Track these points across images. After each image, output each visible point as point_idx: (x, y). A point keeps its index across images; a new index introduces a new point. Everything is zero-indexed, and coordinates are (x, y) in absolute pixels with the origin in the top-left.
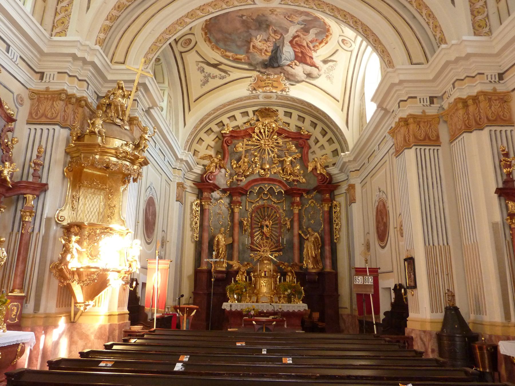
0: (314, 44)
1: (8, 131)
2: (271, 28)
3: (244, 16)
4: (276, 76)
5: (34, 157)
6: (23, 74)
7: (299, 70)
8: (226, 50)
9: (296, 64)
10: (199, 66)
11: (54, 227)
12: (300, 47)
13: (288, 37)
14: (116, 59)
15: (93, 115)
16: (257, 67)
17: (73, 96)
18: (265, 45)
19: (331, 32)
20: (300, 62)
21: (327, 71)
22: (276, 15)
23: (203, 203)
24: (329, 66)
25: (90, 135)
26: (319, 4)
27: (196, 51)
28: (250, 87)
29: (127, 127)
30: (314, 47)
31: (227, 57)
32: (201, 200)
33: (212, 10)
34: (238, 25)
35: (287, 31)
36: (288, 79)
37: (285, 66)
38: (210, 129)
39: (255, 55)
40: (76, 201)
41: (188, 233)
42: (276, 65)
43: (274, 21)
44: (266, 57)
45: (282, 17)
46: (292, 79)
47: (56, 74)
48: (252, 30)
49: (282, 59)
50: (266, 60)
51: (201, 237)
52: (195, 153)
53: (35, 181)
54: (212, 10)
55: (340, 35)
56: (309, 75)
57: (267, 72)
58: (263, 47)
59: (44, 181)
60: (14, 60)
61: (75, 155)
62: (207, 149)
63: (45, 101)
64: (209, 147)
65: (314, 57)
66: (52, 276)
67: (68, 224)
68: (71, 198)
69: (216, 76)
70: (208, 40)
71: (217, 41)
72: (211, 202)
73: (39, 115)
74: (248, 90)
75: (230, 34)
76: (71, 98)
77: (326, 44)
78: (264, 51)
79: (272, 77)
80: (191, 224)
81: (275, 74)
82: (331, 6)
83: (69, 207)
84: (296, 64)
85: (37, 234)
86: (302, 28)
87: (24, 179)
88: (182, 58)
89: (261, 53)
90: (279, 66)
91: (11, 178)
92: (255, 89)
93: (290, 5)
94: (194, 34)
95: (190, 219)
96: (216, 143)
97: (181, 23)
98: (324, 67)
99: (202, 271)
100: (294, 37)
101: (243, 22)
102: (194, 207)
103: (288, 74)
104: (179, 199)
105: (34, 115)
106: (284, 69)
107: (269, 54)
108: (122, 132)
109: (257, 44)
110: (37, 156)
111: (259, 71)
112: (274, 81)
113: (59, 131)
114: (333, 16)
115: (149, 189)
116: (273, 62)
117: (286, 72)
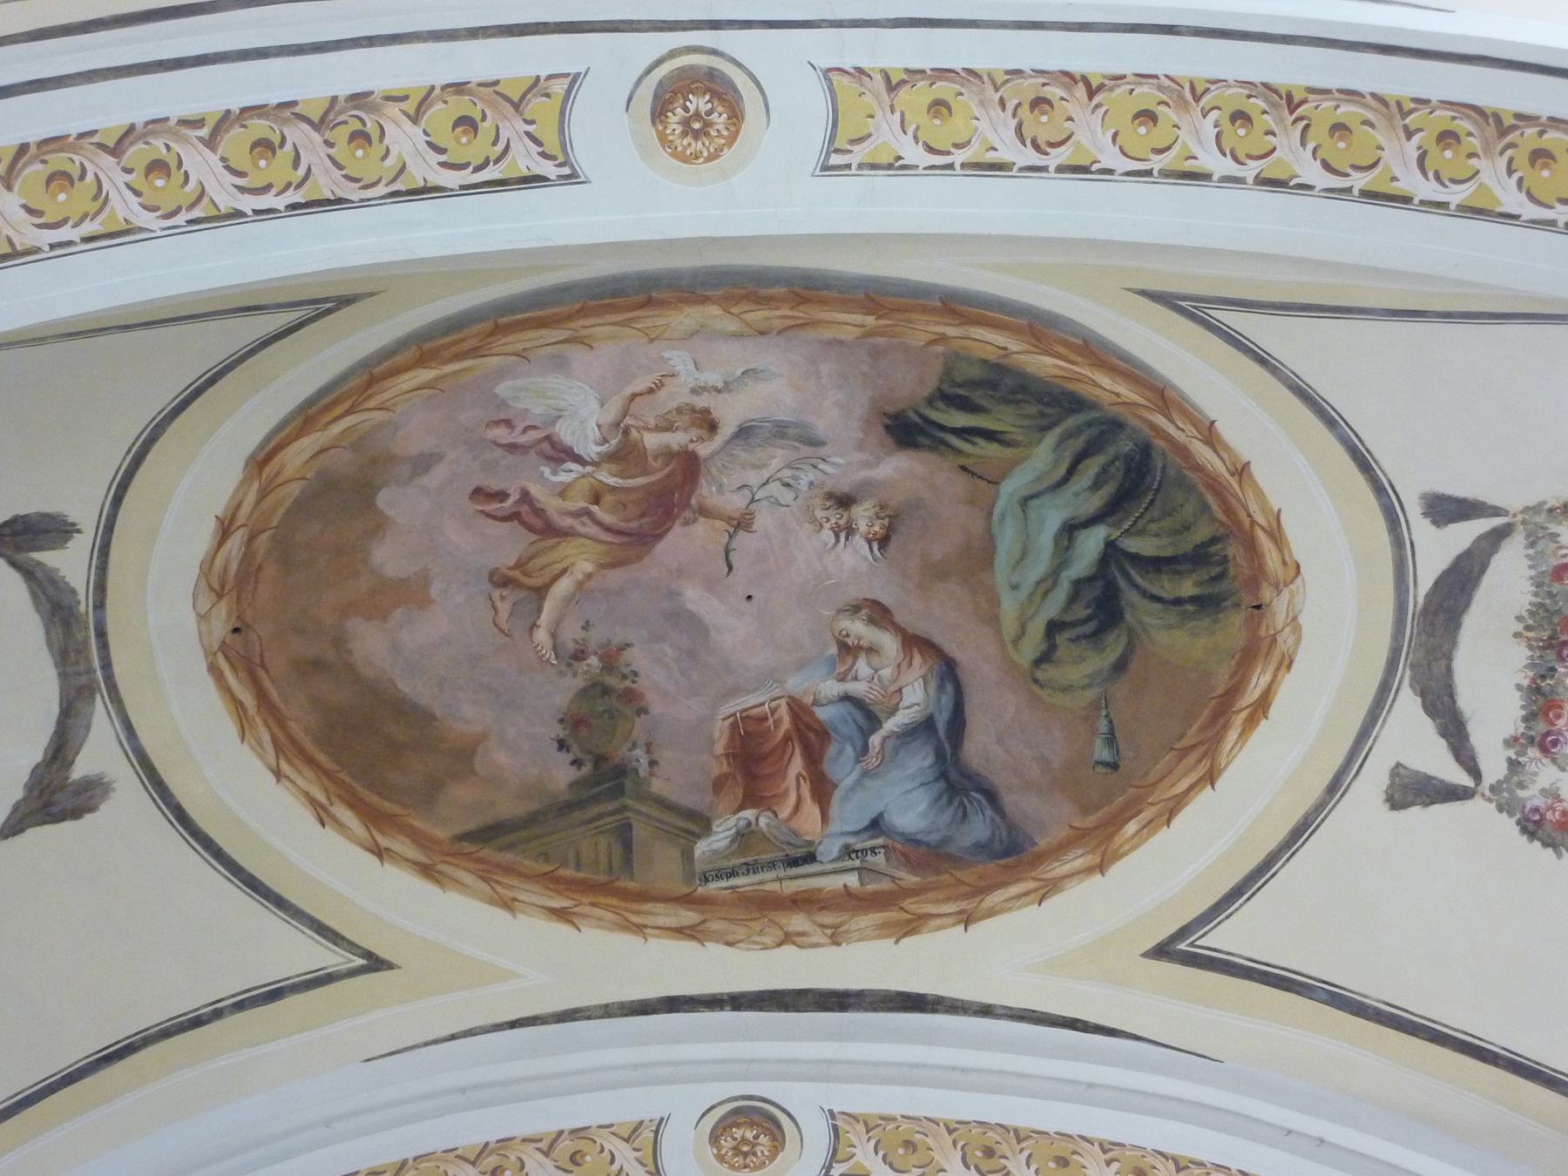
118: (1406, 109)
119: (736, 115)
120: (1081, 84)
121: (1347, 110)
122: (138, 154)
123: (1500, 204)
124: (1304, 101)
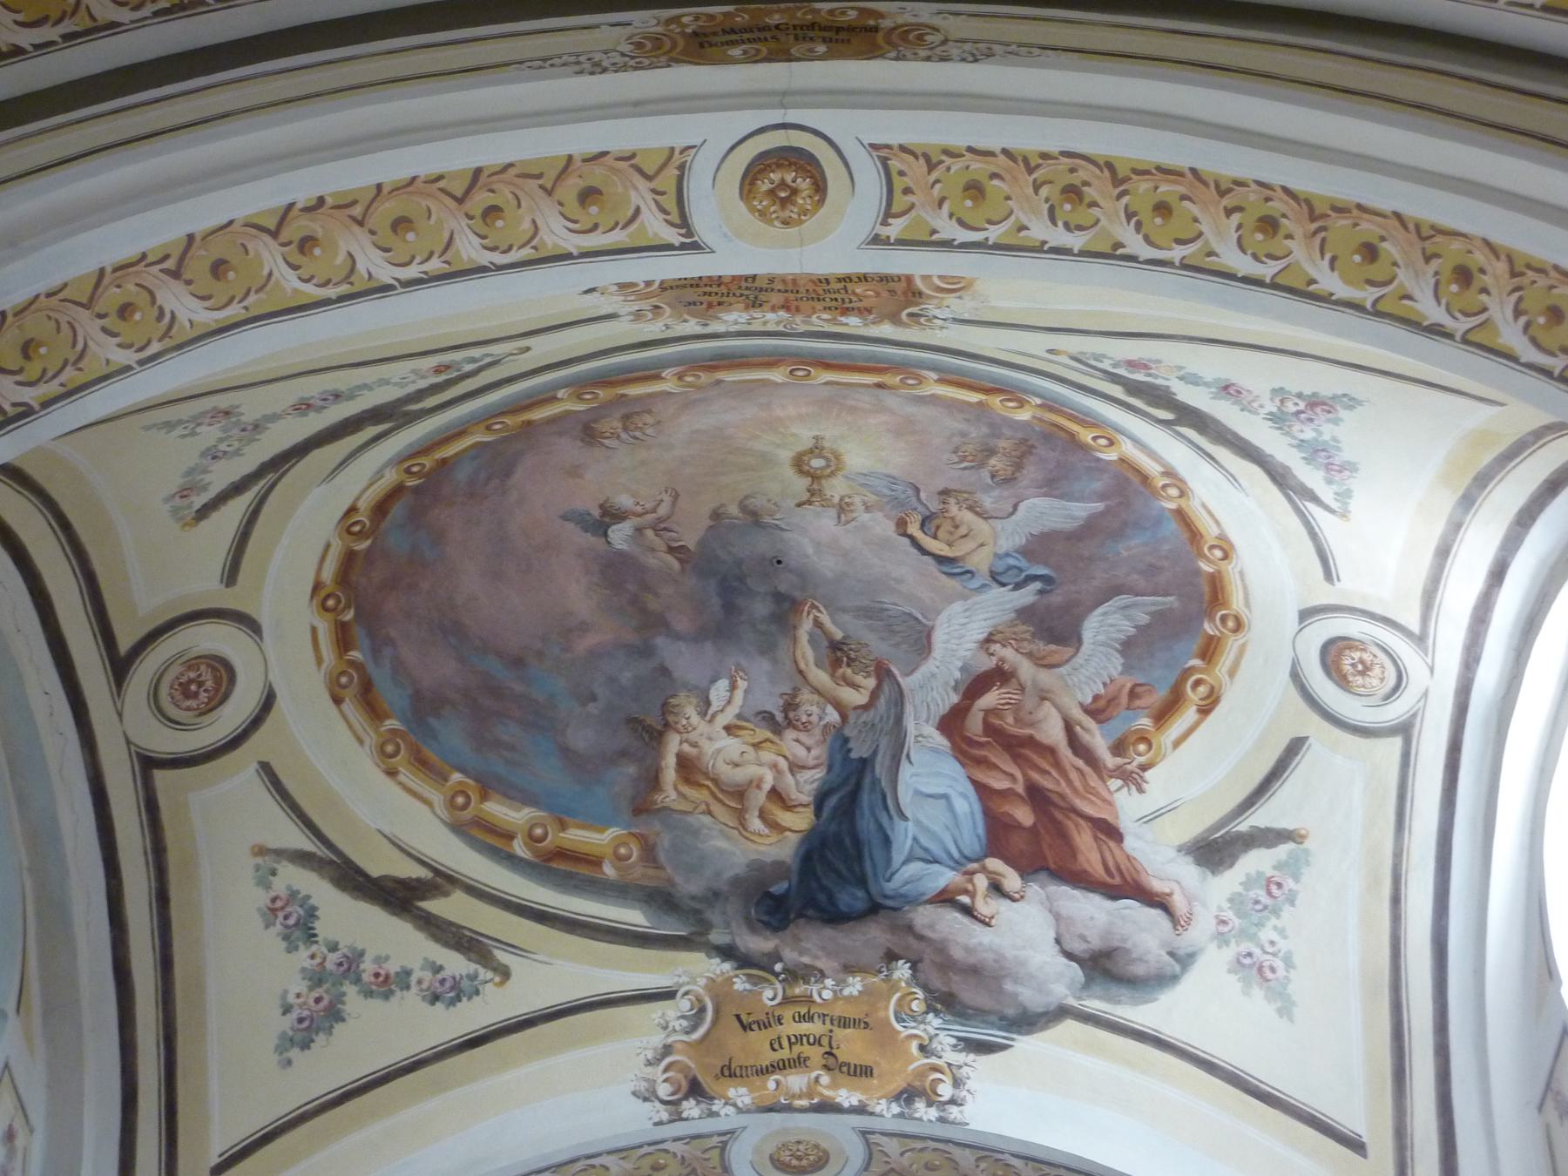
0: (1120, 724)
2: (806, 626)
3: (619, 516)
4: (855, 985)
7: (1026, 929)
8: (487, 786)
9: (997, 888)
10: (279, 886)
12: (1017, 758)
13: (930, 687)
16: (713, 916)
18: (767, 756)
19: (1237, 603)
20: (1030, 867)
21: (1236, 922)
22: (843, 508)
24: (1248, 884)
26: (1163, 209)
27: (266, 769)
28: (657, 1073)
30: (1119, 748)
31: (490, 839)
33: (374, 265)
34: (578, 595)
35: (921, 643)
36: (945, 1002)
37: (915, 901)
39: (696, 833)
42: (850, 898)
43: (827, 565)
44: (775, 843)
45: (884, 526)
46: (988, 1010)
48: (678, 637)
49: (898, 856)
50: (779, 868)
54: (374, 265)
55: (1306, 615)
56: (1103, 966)
57: (790, 955)
58: (751, 771)
65: (1126, 823)
70: (358, 691)
71: (425, 707)
74: (648, 1096)
75: (518, 663)
77: (1205, 711)
78: (759, 798)
79: (824, 992)
81: (849, 969)
82: (1253, 196)
84: (997, 888)
86: (1025, 614)
88: (151, 806)
89: (740, 815)
90: (874, 909)
92: (695, 1089)
93: (947, 245)
94: (250, 624)
97: (125, 311)
98: (1213, 896)
100: (977, 685)
101: (616, 573)
103: (947, 965)
106: (910, 928)
107: (800, 821)
109: (709, 748)
111: (727, 952)
112: (844, 1023)
114: (1274, 286)
116: (832, 879)
117: (929, 955)
118: (1033, 164)
119: (820, 187)
120: (922, 161)
121: (978, 167)
122: (573, 185)
123: (1426, 318)
124: (1038, 166)
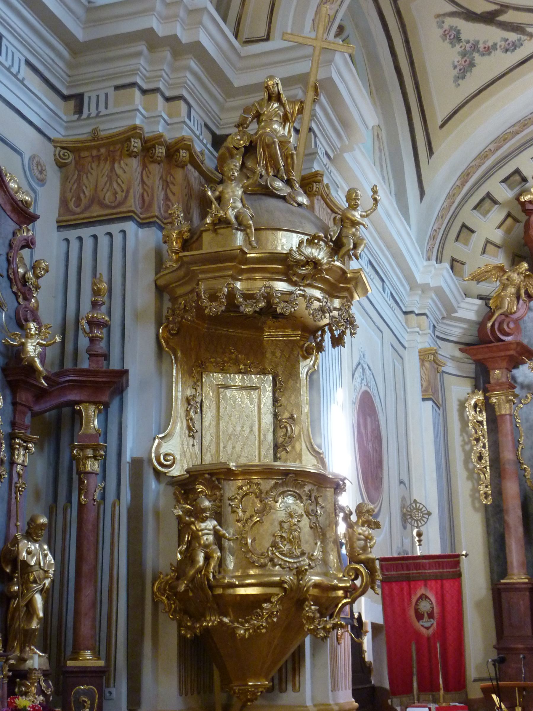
1: (23, 247)
5: (86, 308)
6: (39, 105)
10: (446, 26)
11: (152, 485)
14: (246, 34)
15: (217, 179)
17: (158, 139)
23: (494, 400)
25: (215, 231)
29: (303, 199)
32: (485, 391)
38: (488, 196)
40: (196, 413)
41: (463, 487)
47: (111, 91)
51: (498, 492)
52: (455, 264)
53: (94, 366)
59: (115, 365)
60: (14, 70)
61: (180, 291)
62: (484, 252)
63: (94, 165)
64: (490, 247)
66: (162, 617)
67: (188, 471)
68: (182, 405)
69: (495, 46)
72: (515, 396)
73: (84, 201)
76: (154, 147)
80: (467, 460)
83: (181, 428)
85: (114, 505)
87: (68, 365)
91: (42, 362)
95: (463, 446)
96: (508, 231)
99: (513, 588)
102: (470, 413)
104: (433, 394)
105: (72, 205)
108: (292, 213)
110: (95, 305)
113: (136, 234)
115: (360, 369)
